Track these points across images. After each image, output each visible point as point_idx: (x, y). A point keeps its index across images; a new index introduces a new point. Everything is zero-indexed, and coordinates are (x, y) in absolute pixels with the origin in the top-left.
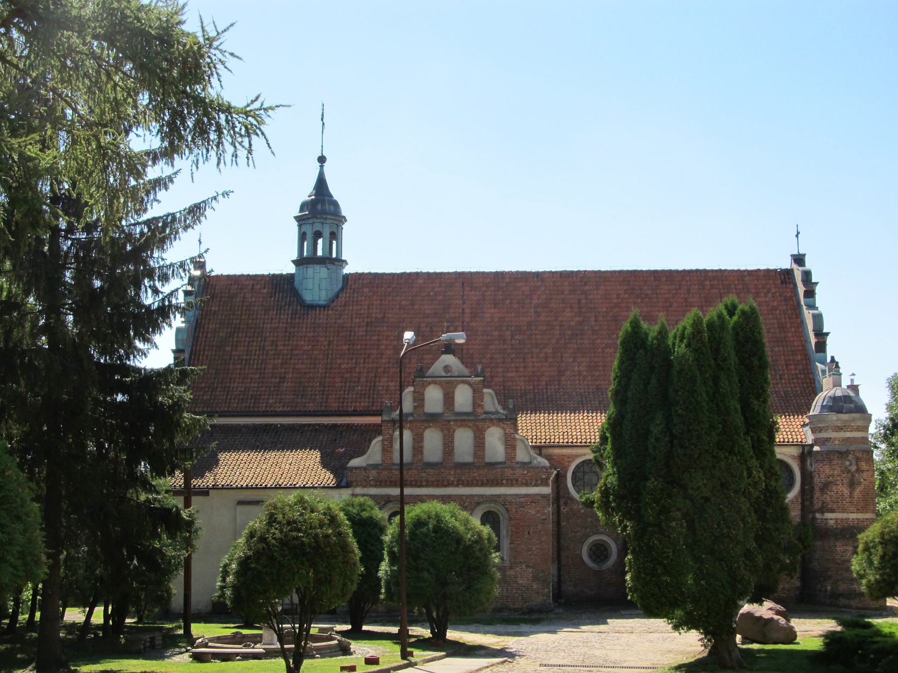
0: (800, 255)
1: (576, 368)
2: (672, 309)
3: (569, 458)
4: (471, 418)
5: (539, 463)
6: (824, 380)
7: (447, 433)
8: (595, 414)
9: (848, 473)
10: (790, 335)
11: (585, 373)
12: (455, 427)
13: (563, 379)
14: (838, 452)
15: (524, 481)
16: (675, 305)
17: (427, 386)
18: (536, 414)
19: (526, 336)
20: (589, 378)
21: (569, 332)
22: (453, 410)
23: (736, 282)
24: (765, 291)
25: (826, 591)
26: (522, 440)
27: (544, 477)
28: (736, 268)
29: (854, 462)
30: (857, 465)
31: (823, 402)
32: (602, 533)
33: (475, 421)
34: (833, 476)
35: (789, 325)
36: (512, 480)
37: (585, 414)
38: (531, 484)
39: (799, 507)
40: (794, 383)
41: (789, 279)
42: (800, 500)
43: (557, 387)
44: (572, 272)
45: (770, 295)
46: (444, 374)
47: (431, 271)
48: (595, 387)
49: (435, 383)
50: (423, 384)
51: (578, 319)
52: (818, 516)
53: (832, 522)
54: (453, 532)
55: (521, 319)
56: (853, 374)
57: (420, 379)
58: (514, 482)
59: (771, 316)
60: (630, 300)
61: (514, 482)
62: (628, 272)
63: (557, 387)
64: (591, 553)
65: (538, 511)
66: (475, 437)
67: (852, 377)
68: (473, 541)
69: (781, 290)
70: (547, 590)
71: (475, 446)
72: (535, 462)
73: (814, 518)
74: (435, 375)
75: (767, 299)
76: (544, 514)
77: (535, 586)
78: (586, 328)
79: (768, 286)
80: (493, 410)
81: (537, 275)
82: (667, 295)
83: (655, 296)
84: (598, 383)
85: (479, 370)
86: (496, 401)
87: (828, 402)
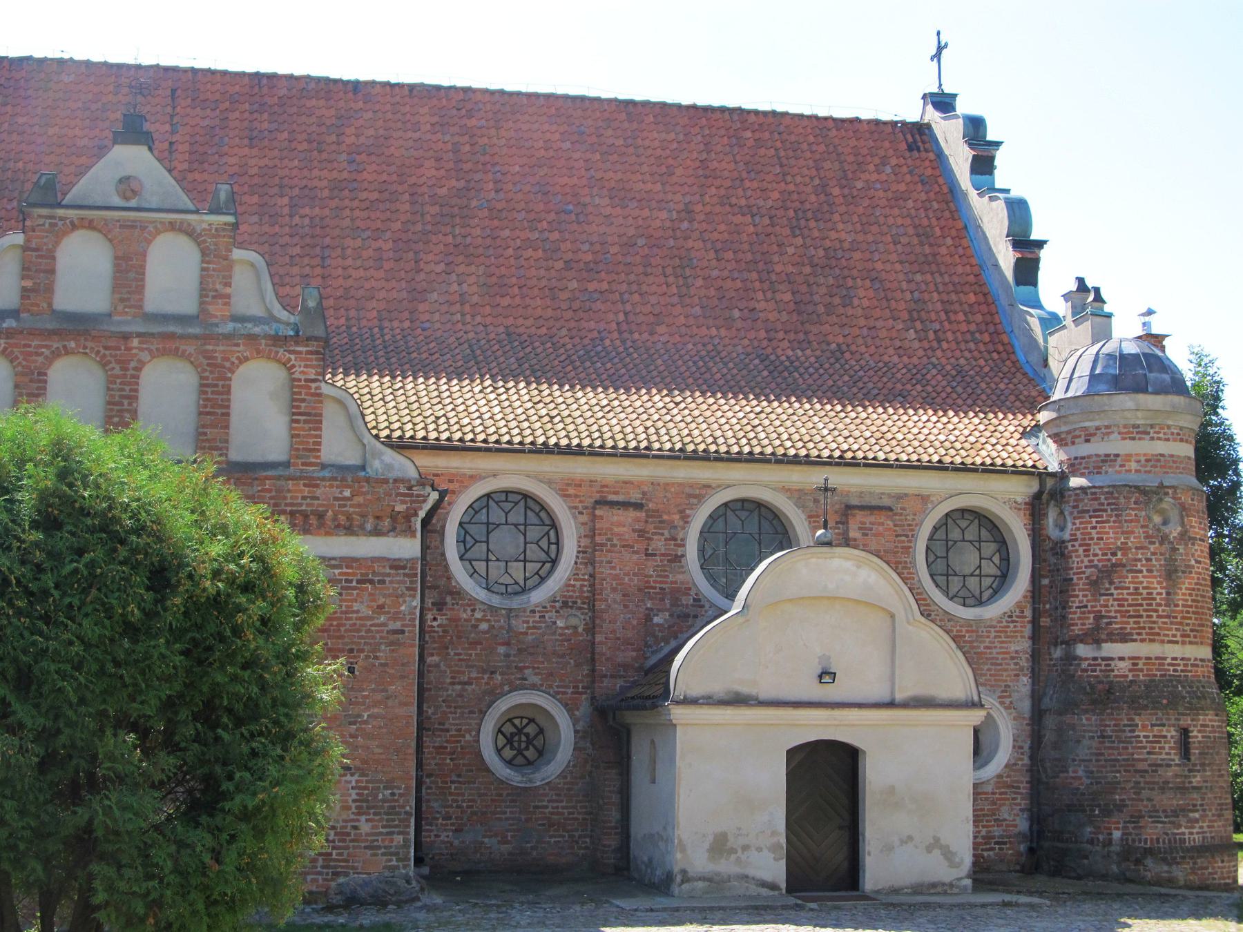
0: (943, 94)
1: (455, 287)
2: (674, 179)
3: (451, 481)
4: (191, 330)
5: (389, 467)
6: (1052, 340)
7: (117, 371)
8: (511, 384)
9: (1161, 543)
10: (944, 251)
11: (475, 299)
12: (145, 356)
13: (421, 307)
14: (1136, 487)
15: (342, 518)
16: (679, 171)
17: (65, 234)
18: (358, 375)
19: (327, 212)
20: (488, 310)
21: (435, 210)
22: (141, 307)
23: (811, 138)
24: (877, 160)
25: (1109, 842)
26: (340, 402)
27: (400, 508)
28: (807, 112)
29: (1174, 515)
30: (1183, 524)
31: (1094, 368)
32: (534, 687)
33: (206, 338)
34: (1124, 548)
35: (938, 232)
36: (306, 516)
37: (488, 382)
38: (362, 527)
39: (1028, 631)
40: (970, 351)
41: (923, 142)
42: (1028, 613)
43: (407, 324)
44: (438, 88)
45: (888, 170)
46: (117, 201)
47: (96, 58)
48: (501, 329)
49: (90, 225)
50: (53, 225)
51: (454, 183)
52: (1082, 650)
53: (1122, 664)
54: (139, 530)
55: (316, 173)
56: (1150, 312)
57: (45, 211)
58: (313, 521)
59: (896, 211)
60: (576, 155)
61: (313, 521)
62: (566, 97)
63: (407, 324)
64: (502, 741)
65: (381, 607)
66: (203, 387)
67: (1147, 319)
68: (231, 581)
69: (909, 162)
70: (399, 839)
71: (200, 413)
72: (377, 464)
73: (1070, 658)
74: (90, 202)
75: (884, 177)
76: (396, 616)
77: (365, 827)
78: (474, 203)
79: (882, 152)
80: (257, 311)
81: (355, 87)
82: (659, 152)
83: (631, 150)
84: (510, 321)
85: (223, 196)
86: (269, 286)
87: (1105, 367)
